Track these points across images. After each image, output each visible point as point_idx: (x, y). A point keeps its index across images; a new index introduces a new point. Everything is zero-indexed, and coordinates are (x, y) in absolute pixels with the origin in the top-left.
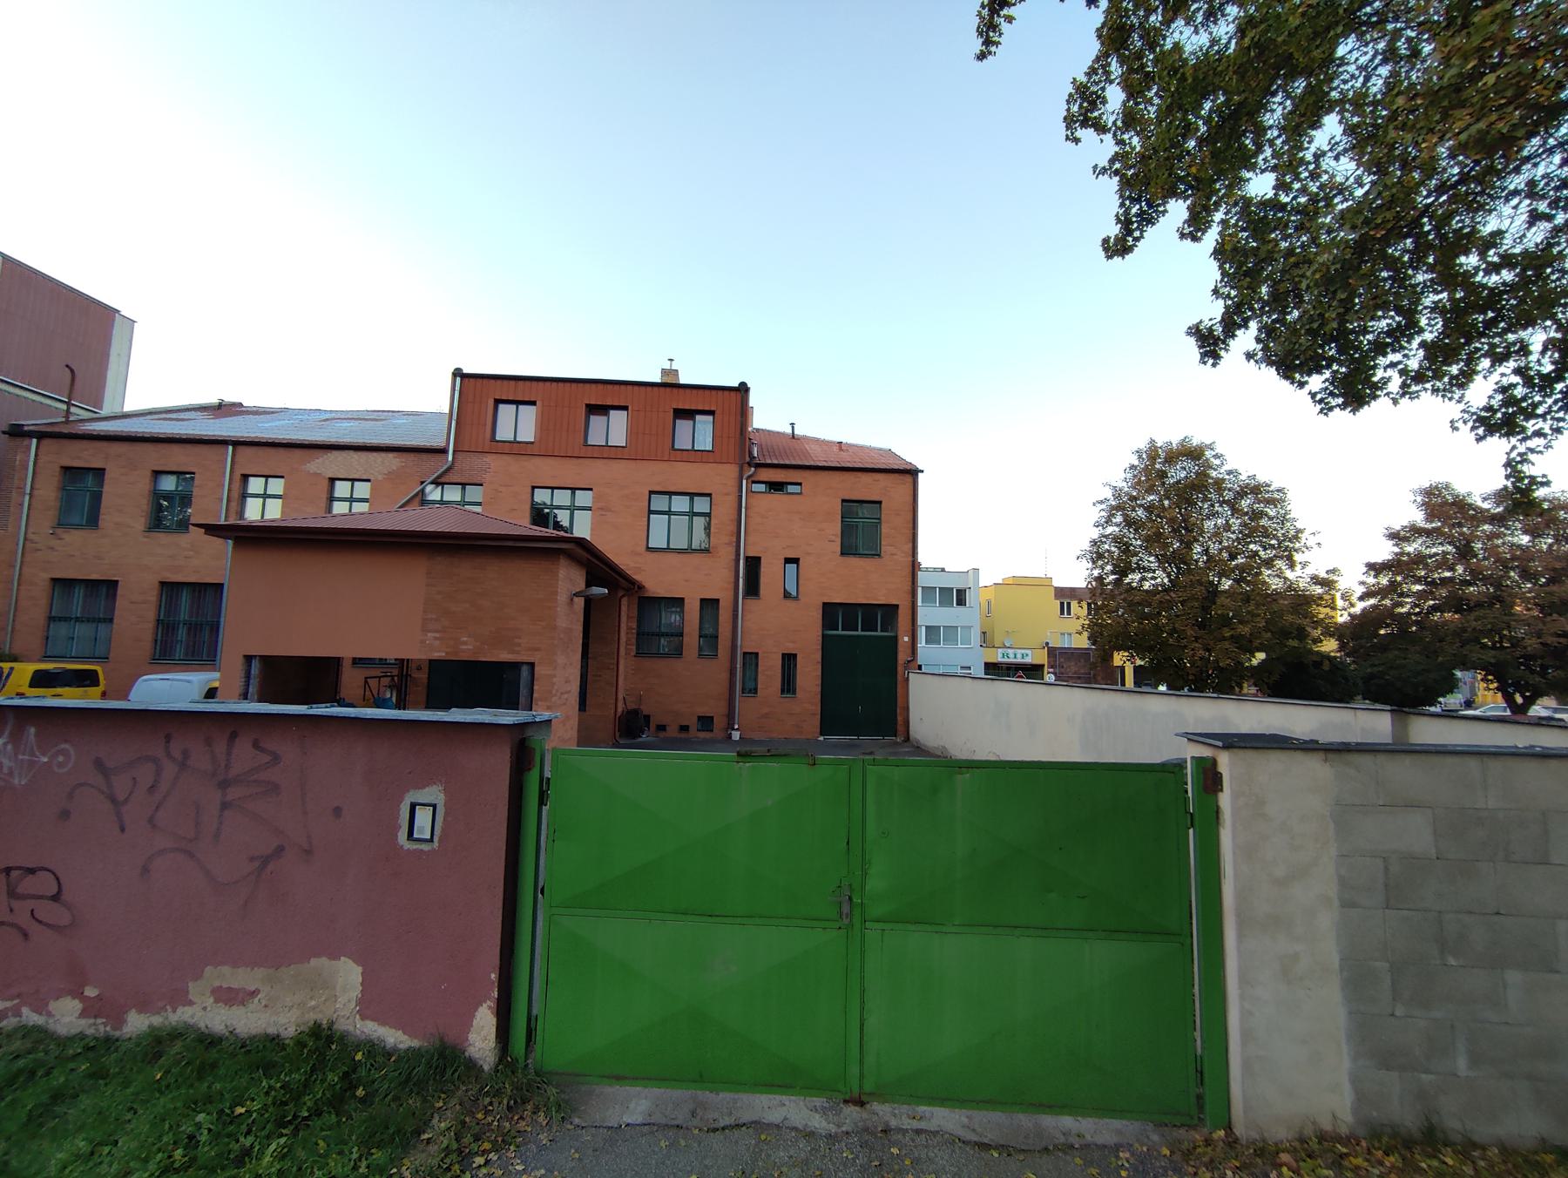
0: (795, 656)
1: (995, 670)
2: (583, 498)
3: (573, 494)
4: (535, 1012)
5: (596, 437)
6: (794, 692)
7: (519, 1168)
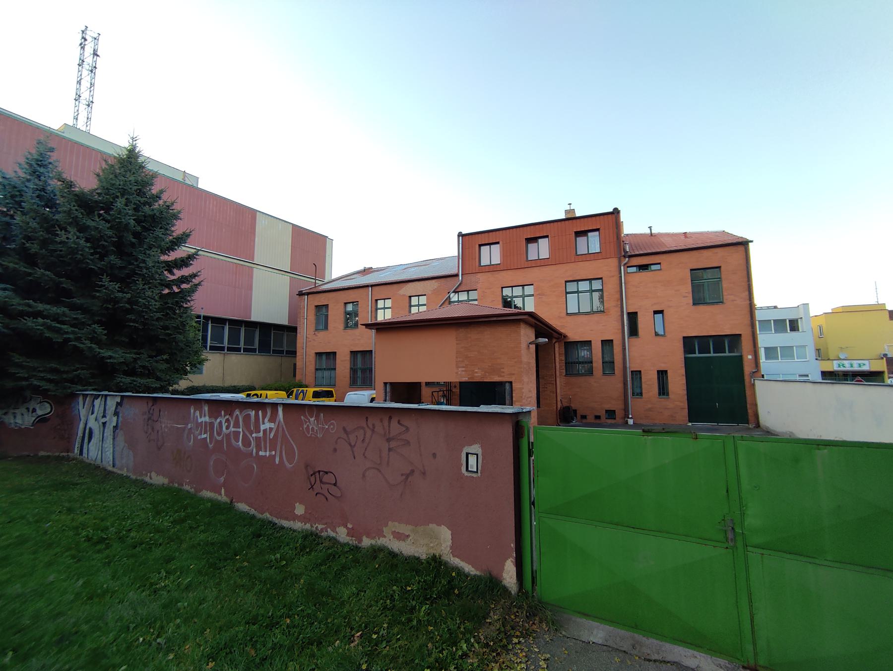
0: (666, 372)
1: (829, 376)
2: (529, 290)
3: (591, 283)
4: (534, 568)
5: (532, 256)
6: (668, 395)
7: (537, 650)
